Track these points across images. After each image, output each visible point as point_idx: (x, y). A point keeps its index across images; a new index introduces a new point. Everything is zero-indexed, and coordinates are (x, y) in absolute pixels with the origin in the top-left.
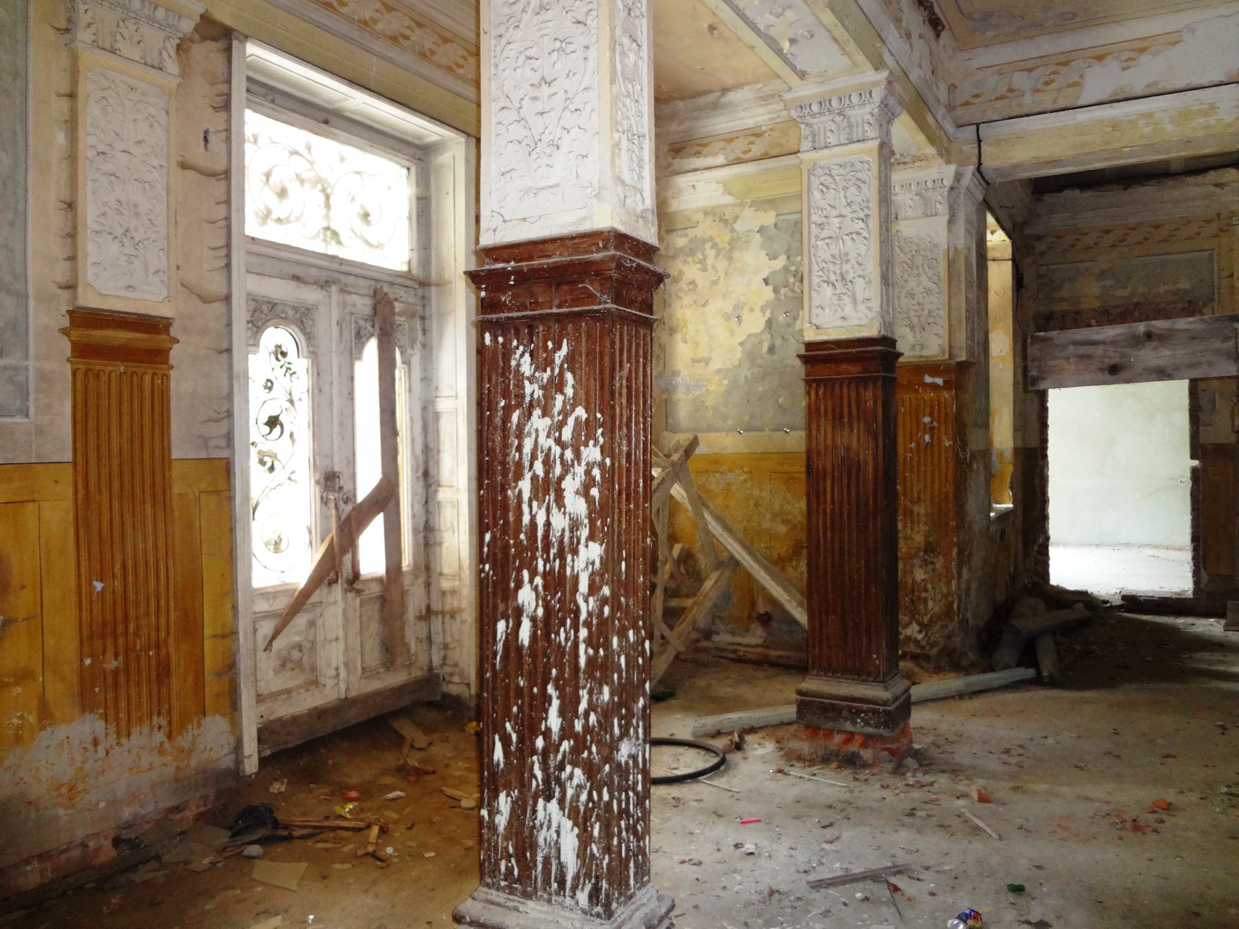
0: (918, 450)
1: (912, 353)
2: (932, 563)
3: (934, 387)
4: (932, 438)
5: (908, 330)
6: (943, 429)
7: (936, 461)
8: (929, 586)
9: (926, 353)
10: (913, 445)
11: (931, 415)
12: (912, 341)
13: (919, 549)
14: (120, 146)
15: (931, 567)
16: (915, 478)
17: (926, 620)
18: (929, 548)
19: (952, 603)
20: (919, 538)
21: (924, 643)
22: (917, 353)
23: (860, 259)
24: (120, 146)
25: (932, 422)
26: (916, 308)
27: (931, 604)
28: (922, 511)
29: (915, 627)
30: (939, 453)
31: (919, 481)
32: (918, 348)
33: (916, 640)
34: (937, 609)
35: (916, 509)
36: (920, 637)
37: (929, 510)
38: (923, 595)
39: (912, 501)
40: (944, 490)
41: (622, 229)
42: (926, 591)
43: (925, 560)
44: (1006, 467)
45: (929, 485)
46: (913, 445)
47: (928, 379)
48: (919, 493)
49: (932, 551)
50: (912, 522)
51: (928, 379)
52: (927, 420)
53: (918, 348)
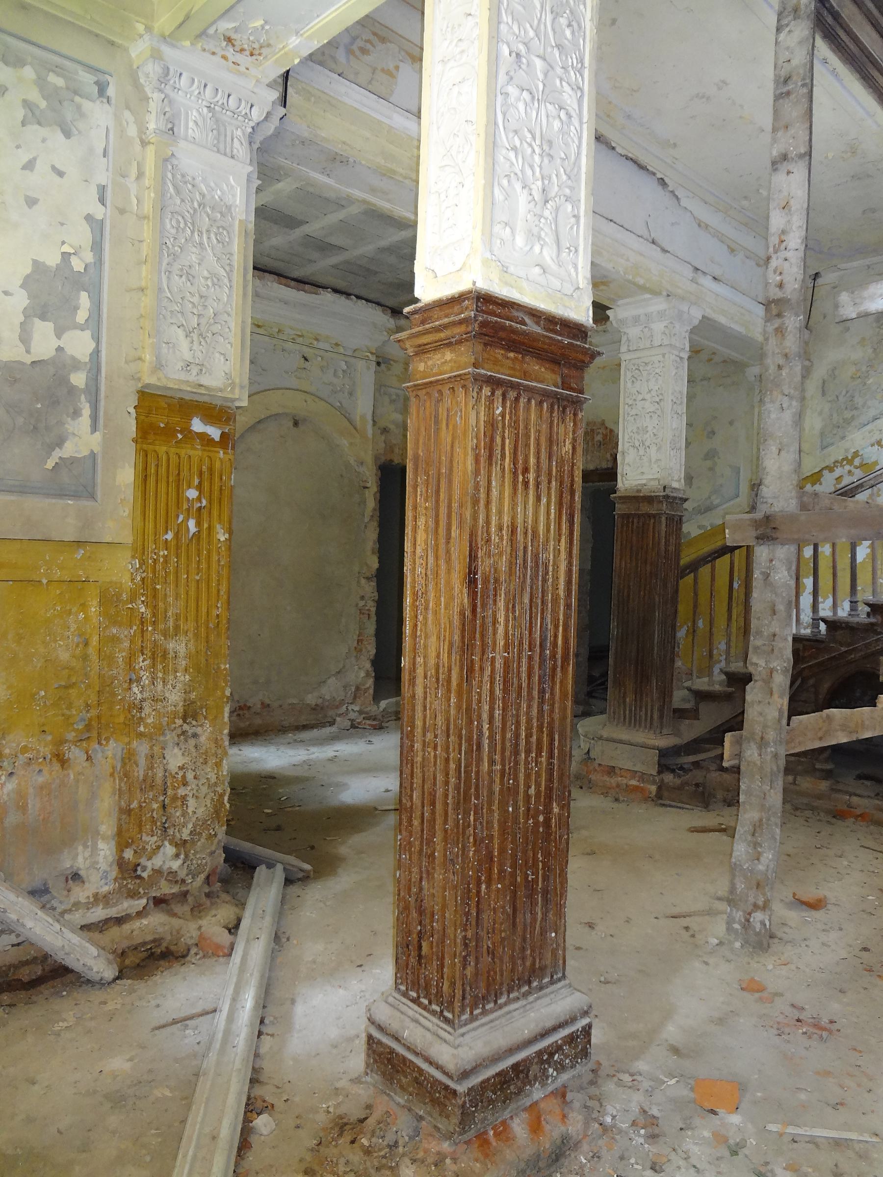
0: (178, 547)
1: (183, 376)
2: (195, 735)
3: (205, 439)
4: (199, 524)
5: (180, 333)
6: (215, 513)
7: (204, 566)
8: (190, 776)
9: (206, 381)
10: (170, 536)
11: (199, 487)
12: (188, 356)
13: (175, 715)
14: (640, 397)
15: (192, 742)
16: (171, 591)
17: (185, 834)
18: (190, 713)
19: (222, 796)
20: (175, 698)
21: (182, 874)
22: (192, 377)
23: (655, 431)
24: (640, 397)
25: (199, 499)
26: (195, 300)
27: (192, 803)
28: (182, 650)
29: (169, 850)
30: (209, 552)
31: (177, 597)
32: (195, 370)
33: (172, 873)
34: (201, 812)
35: (171, 645)
36: (176, 865)
37: (191, 645)
38: (181, 792)
39: (165, 634)
40: (215, 612)
41: (483, 285)
42: (185, 784)
43: (184, 733)
44: (553, 479)
45: (192, 604)
46: (170, 536)
47: (197, 425)
48: (177, 617)
49: (195, 717)
50: (165, 671)
51: (197, 425)
52: (192, 494)
53: (195, 370)
